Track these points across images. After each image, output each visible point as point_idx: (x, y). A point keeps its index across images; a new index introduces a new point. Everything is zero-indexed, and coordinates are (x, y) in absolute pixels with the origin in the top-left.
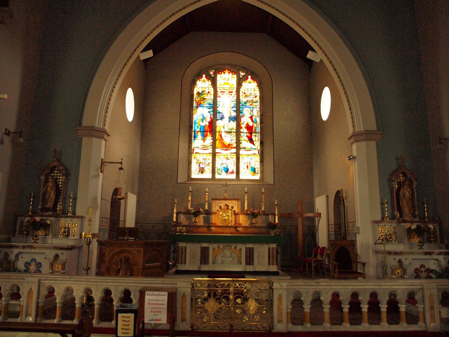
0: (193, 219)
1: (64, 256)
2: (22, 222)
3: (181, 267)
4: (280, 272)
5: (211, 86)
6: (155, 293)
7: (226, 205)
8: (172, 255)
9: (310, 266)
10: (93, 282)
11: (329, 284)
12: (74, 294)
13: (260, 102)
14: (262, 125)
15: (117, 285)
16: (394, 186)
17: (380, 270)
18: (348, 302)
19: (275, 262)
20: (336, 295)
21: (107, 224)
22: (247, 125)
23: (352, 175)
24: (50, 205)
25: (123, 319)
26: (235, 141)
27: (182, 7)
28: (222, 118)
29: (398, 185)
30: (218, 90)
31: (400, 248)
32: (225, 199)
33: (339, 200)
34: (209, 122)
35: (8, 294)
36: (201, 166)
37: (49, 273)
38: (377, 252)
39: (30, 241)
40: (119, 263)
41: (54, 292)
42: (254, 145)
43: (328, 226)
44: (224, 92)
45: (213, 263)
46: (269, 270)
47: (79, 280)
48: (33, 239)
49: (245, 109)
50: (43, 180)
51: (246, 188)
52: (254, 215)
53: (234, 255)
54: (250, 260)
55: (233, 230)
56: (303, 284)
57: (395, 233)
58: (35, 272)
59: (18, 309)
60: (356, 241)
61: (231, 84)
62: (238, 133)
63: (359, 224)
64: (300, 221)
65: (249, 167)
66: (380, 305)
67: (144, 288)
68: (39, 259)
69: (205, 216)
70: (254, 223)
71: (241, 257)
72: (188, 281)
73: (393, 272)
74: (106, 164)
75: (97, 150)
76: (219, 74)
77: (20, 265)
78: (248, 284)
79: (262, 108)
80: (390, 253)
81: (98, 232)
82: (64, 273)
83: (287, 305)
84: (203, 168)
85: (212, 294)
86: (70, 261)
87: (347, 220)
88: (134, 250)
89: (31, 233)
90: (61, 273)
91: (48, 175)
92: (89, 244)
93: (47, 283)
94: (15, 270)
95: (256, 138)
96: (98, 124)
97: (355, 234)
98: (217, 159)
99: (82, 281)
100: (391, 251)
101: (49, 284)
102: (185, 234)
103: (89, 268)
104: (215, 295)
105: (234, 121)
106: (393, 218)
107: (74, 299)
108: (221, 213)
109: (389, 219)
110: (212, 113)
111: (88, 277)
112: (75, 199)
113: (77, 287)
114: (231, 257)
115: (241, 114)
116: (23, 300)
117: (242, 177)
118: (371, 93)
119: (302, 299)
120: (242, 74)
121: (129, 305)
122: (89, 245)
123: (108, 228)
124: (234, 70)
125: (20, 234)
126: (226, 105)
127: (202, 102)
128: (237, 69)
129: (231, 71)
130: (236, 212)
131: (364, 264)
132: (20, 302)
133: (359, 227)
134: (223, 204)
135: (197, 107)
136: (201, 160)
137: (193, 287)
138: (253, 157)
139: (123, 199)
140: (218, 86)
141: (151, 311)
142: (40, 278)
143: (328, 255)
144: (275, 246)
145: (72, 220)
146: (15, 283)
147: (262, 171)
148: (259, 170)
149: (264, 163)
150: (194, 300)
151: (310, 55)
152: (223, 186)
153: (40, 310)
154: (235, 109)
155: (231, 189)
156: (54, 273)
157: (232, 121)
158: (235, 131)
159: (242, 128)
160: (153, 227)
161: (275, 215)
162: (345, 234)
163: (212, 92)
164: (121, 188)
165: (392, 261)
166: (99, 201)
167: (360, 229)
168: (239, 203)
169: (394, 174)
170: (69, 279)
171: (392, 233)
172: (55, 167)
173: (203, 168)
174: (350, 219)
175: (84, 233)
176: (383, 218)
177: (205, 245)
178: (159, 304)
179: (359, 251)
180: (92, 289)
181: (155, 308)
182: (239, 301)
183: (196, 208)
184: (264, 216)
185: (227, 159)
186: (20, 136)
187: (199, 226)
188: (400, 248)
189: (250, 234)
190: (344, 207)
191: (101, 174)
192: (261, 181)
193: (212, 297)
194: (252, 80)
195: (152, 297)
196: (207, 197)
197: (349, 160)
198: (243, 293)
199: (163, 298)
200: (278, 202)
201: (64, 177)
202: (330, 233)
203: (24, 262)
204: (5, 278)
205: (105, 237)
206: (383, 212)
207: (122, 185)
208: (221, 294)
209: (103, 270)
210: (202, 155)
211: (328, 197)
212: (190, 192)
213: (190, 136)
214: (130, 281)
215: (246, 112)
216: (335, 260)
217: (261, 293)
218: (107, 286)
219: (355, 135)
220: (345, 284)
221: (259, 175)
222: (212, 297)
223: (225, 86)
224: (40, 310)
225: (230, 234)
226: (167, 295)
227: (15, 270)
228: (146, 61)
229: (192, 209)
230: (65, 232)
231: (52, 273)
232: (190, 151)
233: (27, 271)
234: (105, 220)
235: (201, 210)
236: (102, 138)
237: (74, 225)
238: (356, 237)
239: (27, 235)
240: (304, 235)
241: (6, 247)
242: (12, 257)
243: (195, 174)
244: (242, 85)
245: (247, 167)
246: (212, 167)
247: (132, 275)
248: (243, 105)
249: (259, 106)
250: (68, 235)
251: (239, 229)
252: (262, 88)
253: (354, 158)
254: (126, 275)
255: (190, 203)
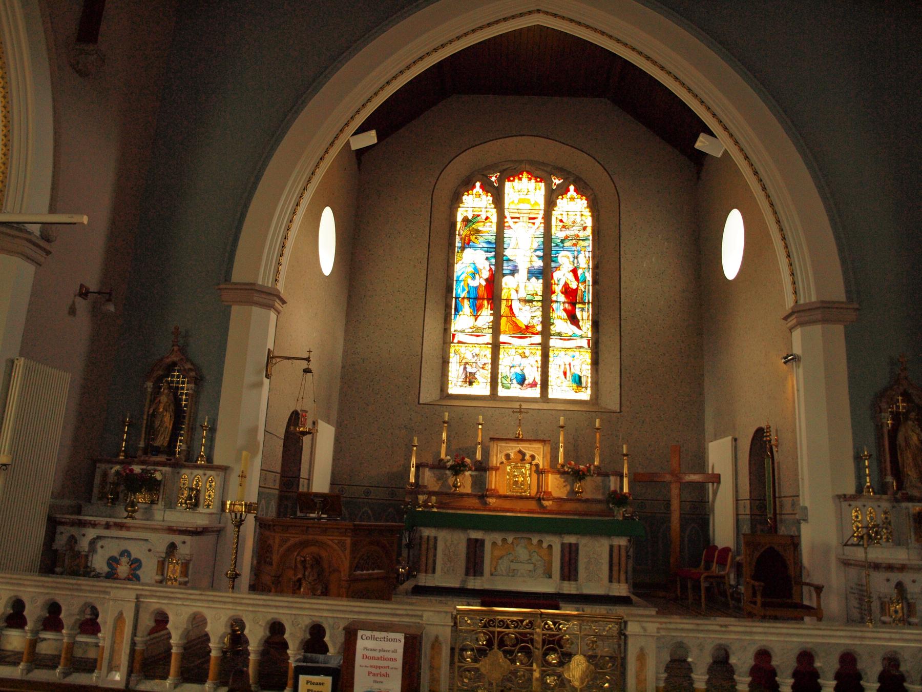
0: (451, 481)
1: (186, 547)
2: (105, 475)
3: (425, 580)
4: (634, 598)
5: (493, 206)
6: (377, 634)
7: (520, 452)
8: (405, 553)
9: (697, 588)
10: (248, 605)
11: (748, 629)
12: (208, 629)
13: (593, 240)
14: (597, 287)
15: (297, 613)
16: (884, 421)
17: (854, 603)
18: (790, 671)
19: (623, 577)
20: (763, 655)
21: (274, 483)
22: (566, 285)
23: (789, 392)
24: (162, 440)
25: (311, 687)
26: (540, 319)
27: (454, 37)
28: (514, 272)
29: (893, 419)
30: (506, 213)
31: (899, 555)
32: (517, 440)
33: (762, 447)
34: (486, 280)
35: (75, 623)
36: (469, 369)
37: (157, 582)
38: (846, 563)
39: (121, 515)
40: (299, 566)
41: (167, 622)
42: (579, 327)
43: (737, 504)
44: (519, 218)
45: (492, 575)
46: (611, 594)
47: (216, 599)
48: (127, 511)
49: (562, 254)
50: (149, 390)
51: (562, 418)
52: (578, 475)
53: (535, 557)
54: (569, 570)
55: (533, 505)
56: (691, 627)
57: (887, 522)
58: (128, 579)
59: (92, 654)
60: (799, 536)
61: (532, 202)
63: (805, 500)
64: (675, 491)
65: (568, 374)
66: (862, 682)
67: (355, 622)
68: (137, 551)
69: (474, 473)
70: (578, 492)
71: (550, 563)
72: (446, 612)
73: (883, 609)
74: (278, 360)
75: (259, 332)
76: (509, 181)
77: (99, 562)
78: (569, 621)
79: (597, 252)
80: (876, 566)
81: (256, 501)
82: (186, 583)
83: (657, 673)
84: (472, 375)
85: (496, 642)
86: (197, 561)
87: (780, 492)
88: (332, 540)
89: (121, 496)
90: (180, 584)
91: (160, 379)
92: (239, 523)
93: (154, 603)
94: (87, 572)
95: (584, 315)
96: (263, 279)
97: (798, 522)
98: (501, 356)
99: (225, 603)
100: (880, 561)
101: (157, 606)
102: (435, 510)
103: (237, 575)
104: (502, 644)
105: (537, 278)
106: (882, 489)
107: (206, 638)
108: (509, 468)
109: (873, 491)
110: (493, 261)
111: (234, 595)
112: (212, 430)
113: (215, 613)
114: (529, 562)
115: (553, 265)
116: (105, 636)
117: (553, 394)
118: (832, 220)
119: (690, 660)
121: (321, 657)
122: (238, 526)
123: (277, 492)
124: (540, 173)
125: (100, 499)
126: (523, 245)
127: (472, 238)
128: (546, 172)
129: (533, 176)
130: (541, 467)
131: (819, 589)
132: (98, 638)
133: (806, 508)
134: (512, 449)
135: (463, 249)
136: (469, 357)
137: (455, 623)
138: (577, 353)
139: (309, 433)
140: (506, 206)
141: (369, 673)
142: (139, 592)
143: (739, 566)
144: (623, 542)
145: (205, 475)
146: (89, 600)
147: (595, 384)
148: (589, 380)
149: (601, 366)
150: (456, 652)
151: (702, 143)
152: (514, 412)
153: (138, 658)
154: (540, 253)
155: (532, 420)
156: (173, 581)
157: (533, 279)
158: (540, 298)
159: (554, 292)
160: (367, 493)
161: (622, 477)
162: (774, 519)
163: (494, 218)
164: (306, 412)
165: (881, 584)
166: (261, 437)
167: (809, 513)
168: (548, 448)
170: (198, 597)
171: (879, 522)
172: (174, 364)
173: (472, 375)
174: (786, 490)
175: (229, 502)
176: (860, 489)
177: (475, 535)
178: (385, 659)
179: (806, 561)
180: (244, 619)
181: (376, 667)
182: (553, 658)
183: (457, 456)
184: (600, 479)
185: (523, 356)
186: (109, 300)
187: (462, 495)
188: (899, 555)
189: (570, 514)
190: (773, 463)
191: (266, 381)
192: (593, 405)
193: (496, 646)
194: (578, 194)
195: (370, 644)
196: (480, 434)
197: (785, 363)
198: (562, 642)
199: (395, 645)
200: (628, 449)
201: (192, 385)
202: (740, 517)
203: (107, 557)
204: (70, 589)
205: (271, 512)
206: (860, 477)
207: (308, 405)
208: (514, 642)
209: (267, 579)
210: (470, 348)
211: (736, 440)
212: (445, 422)
213: (448, 306)
214: (325, 607)
215: (564, 260)
216: (755, 577)
217: (600, 643)
218: (276, 616)
219: (798, 312)
220: (785, 631)
221: (589, 391)
222: (496, 646)
223: (521, 206)
224: (138, 658)
225: (528, 512)
226: (403, 640)
227: (87, 572)
228: (360, 152)
229: (449, 457)
230: (191, 499)
231: (161, 582)
232: (447, 338)
233: (111, 576)
234: (271, 476)
235: (467, 460)
236: (270, 307)
237: (208, 484)
238: (799, 530)
239: (114, 501)
240: (684, 521)
241: (73, 524)
242: (84, 545)
243: (456, 387)
244: (555, 205)
245: (565, 374)
246: (492, 373)
247: (325, 593)
248: (557, 245)
249: (590, 249)
250: (196, 505)
251: (545, 503)
252: (598, 210)
253: (796, 359)
254: (313, 593)
255: (444, 446)
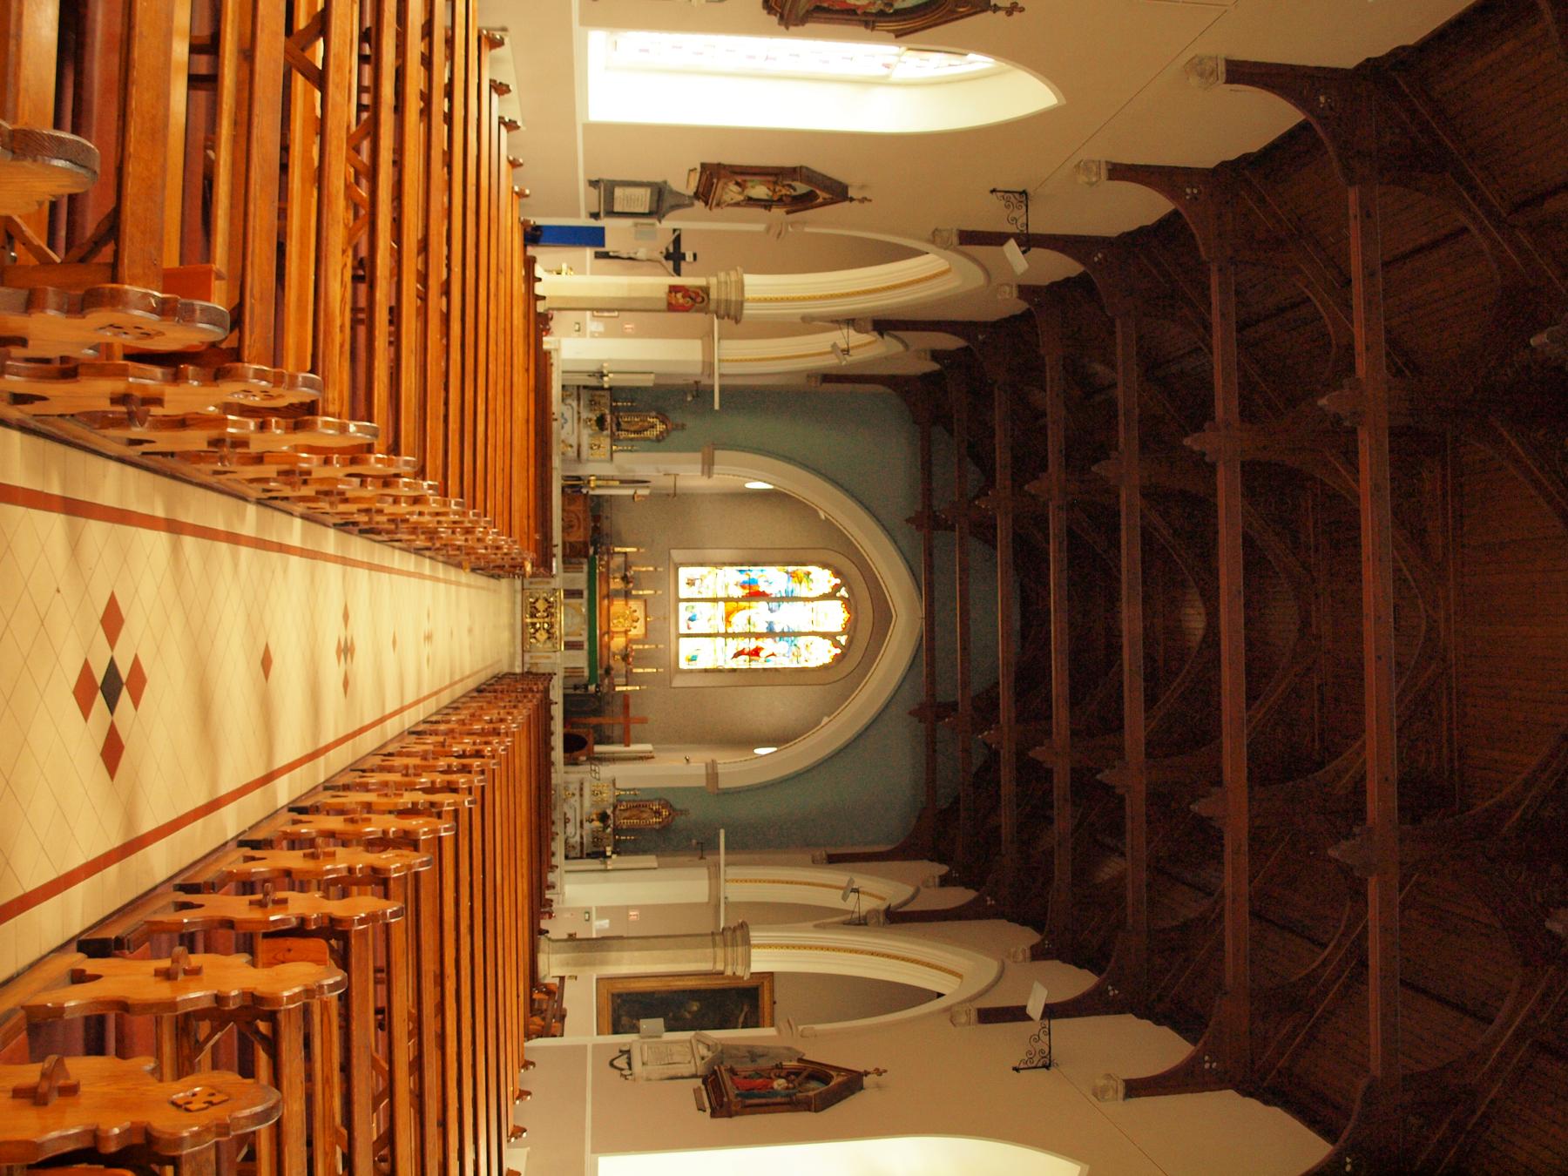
28: (771, 610)
55: (605, 629)
62: (748, 635)
95: (742, 663)
96: (716, 468)
117: (682, 640)
120: (843, 639)
126: (787, 617)
134: (640, 614)
136: (705, 583)
144: (586, 673)
147: (691, 671)
169: (667, 805)
177: (586, 594)
188: (587, 803)
215: (781, 647)
232: (719, 564)
243: (685, 573)
